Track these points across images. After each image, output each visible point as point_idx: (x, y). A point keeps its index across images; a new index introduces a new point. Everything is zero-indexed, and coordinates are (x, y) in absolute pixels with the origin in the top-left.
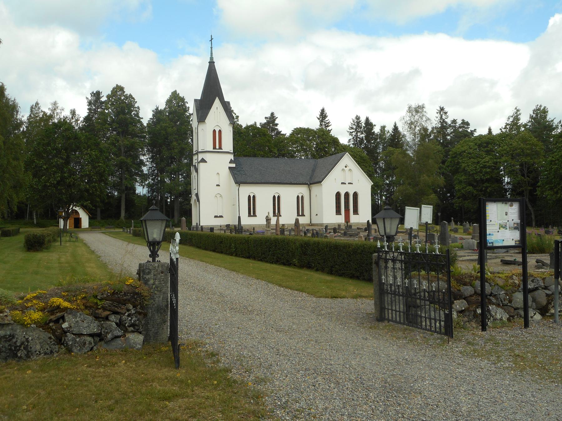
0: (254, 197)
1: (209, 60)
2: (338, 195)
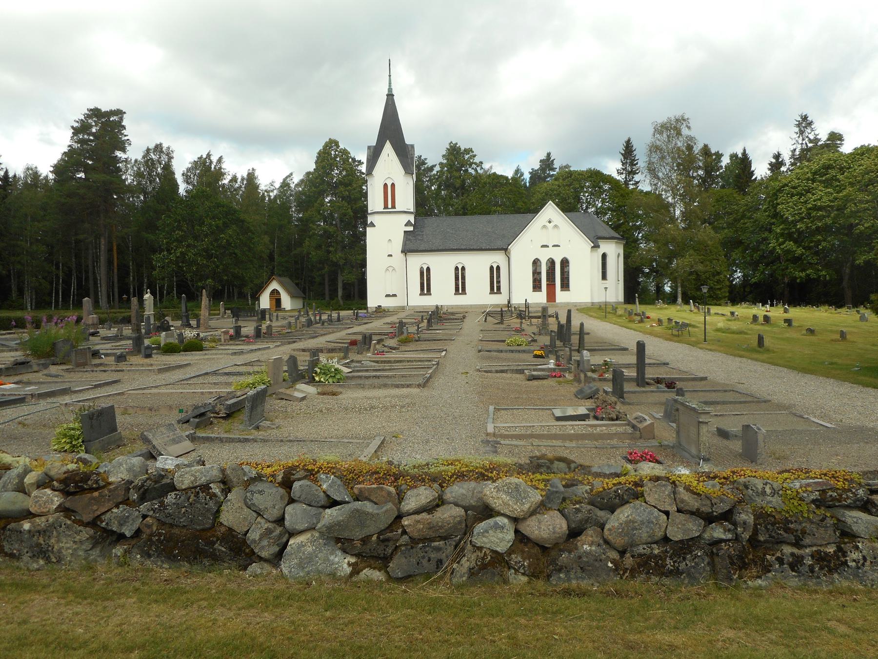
0: (428, 269)
1: (387, 92)
2: (536, 263)
